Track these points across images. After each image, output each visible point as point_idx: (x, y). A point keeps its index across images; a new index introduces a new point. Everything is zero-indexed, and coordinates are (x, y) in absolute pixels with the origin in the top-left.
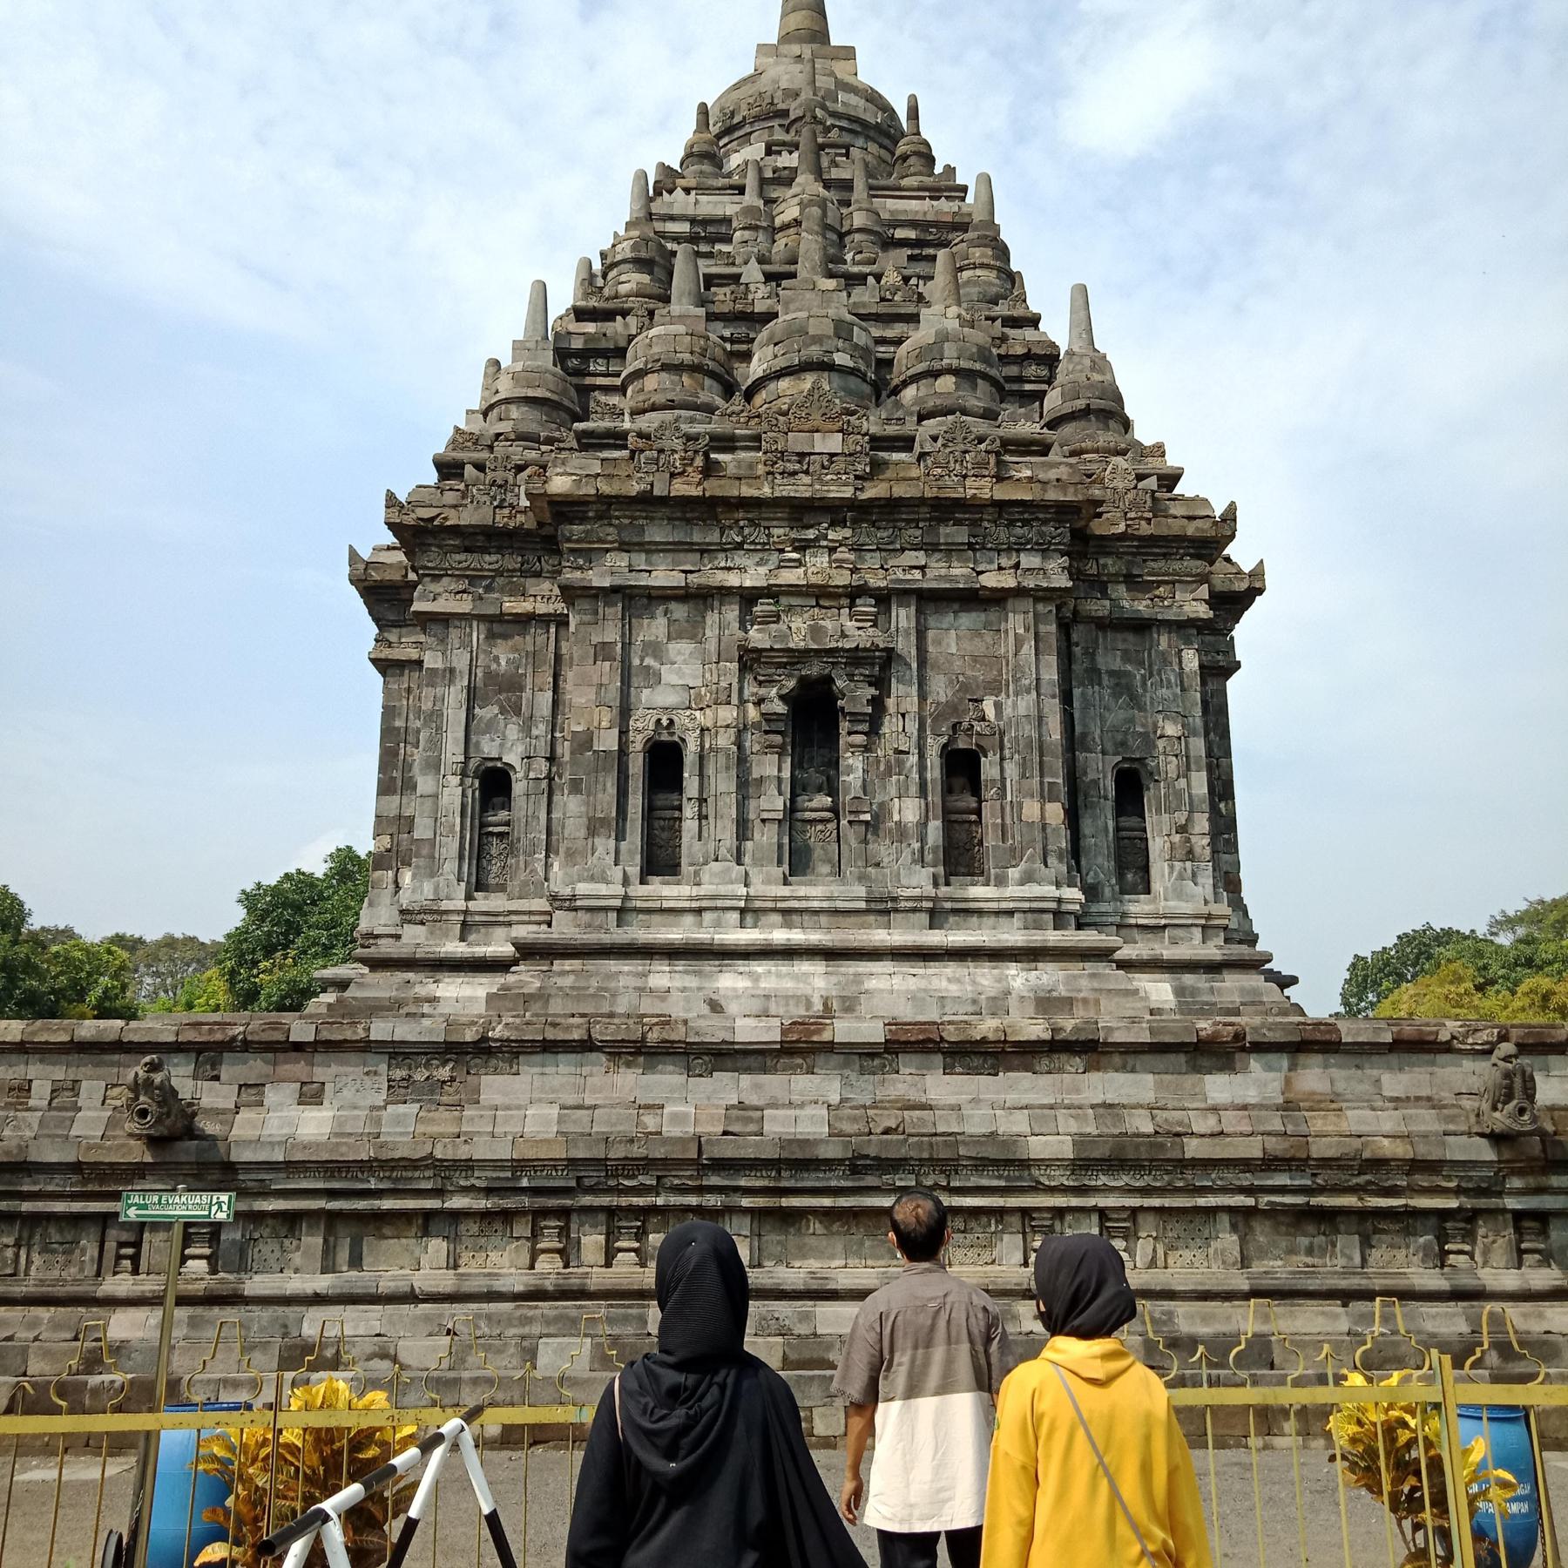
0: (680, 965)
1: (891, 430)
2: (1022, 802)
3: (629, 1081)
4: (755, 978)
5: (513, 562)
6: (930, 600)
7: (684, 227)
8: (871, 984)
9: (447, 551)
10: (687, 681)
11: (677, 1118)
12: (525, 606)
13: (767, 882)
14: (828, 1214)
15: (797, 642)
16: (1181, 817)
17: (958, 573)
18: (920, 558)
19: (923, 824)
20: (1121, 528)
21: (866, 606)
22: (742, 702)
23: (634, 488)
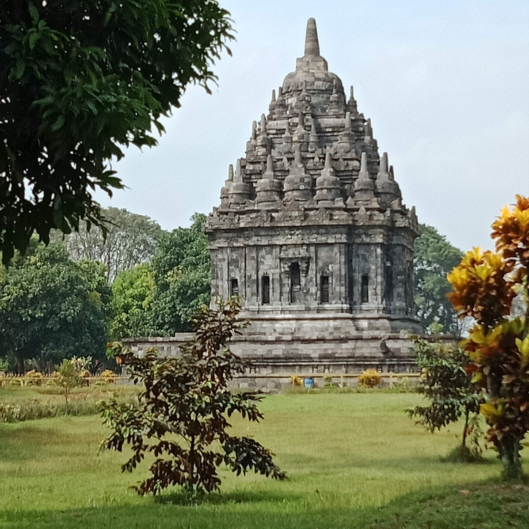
0: (269, 322)
1: (311, 206)
2: (337, 287)
3: (253, 346)
4: (282, 324)
5: (235, 235)
6: (318, 245)
7: (274, 132)
8: (304, 325)
9: (221, 233)
10: (270, 265)
11: (259, 352)
12: (238, 245)
13: (286, 305)
14: (283, 366)
15: (290, 256)
16: (374, 286)
17: (323, 239)
18: (316, 236)
19: (316, 293)
20: (362, 224)
21: (305, 247)
22: (281, 267)
23: (257, 225)
